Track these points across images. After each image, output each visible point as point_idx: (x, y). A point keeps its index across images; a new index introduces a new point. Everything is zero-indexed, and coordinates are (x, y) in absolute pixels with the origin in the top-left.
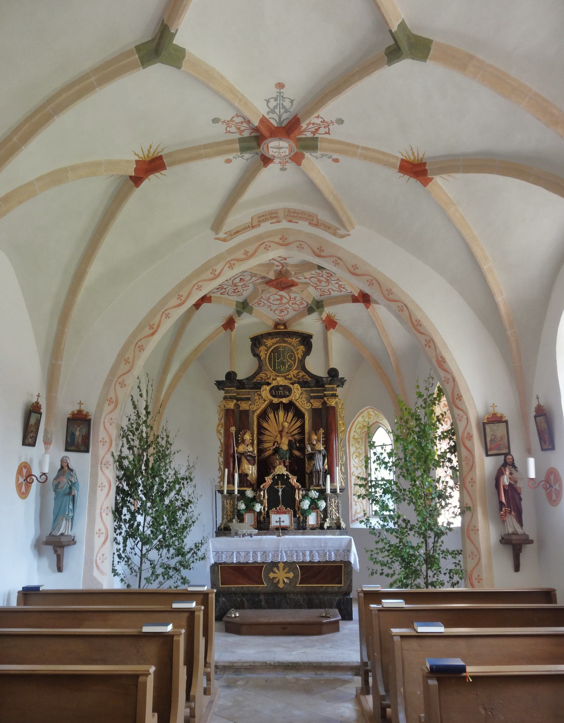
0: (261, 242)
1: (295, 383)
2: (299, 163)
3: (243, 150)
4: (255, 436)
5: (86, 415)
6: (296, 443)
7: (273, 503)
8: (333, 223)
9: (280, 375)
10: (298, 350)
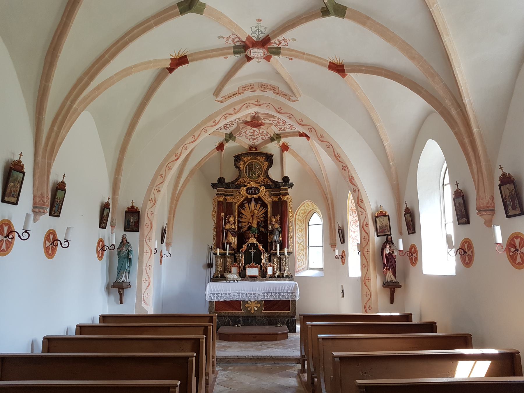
0: (244, 104)
1: (262, 186)
2: (269, 61)
3: (235, 53)
4: (236, 218)
5: (137, 209)
6: (262, 223)
7: (248, 261)
8: (289, 93)
9: (253, 180)
10: (264, 164)
